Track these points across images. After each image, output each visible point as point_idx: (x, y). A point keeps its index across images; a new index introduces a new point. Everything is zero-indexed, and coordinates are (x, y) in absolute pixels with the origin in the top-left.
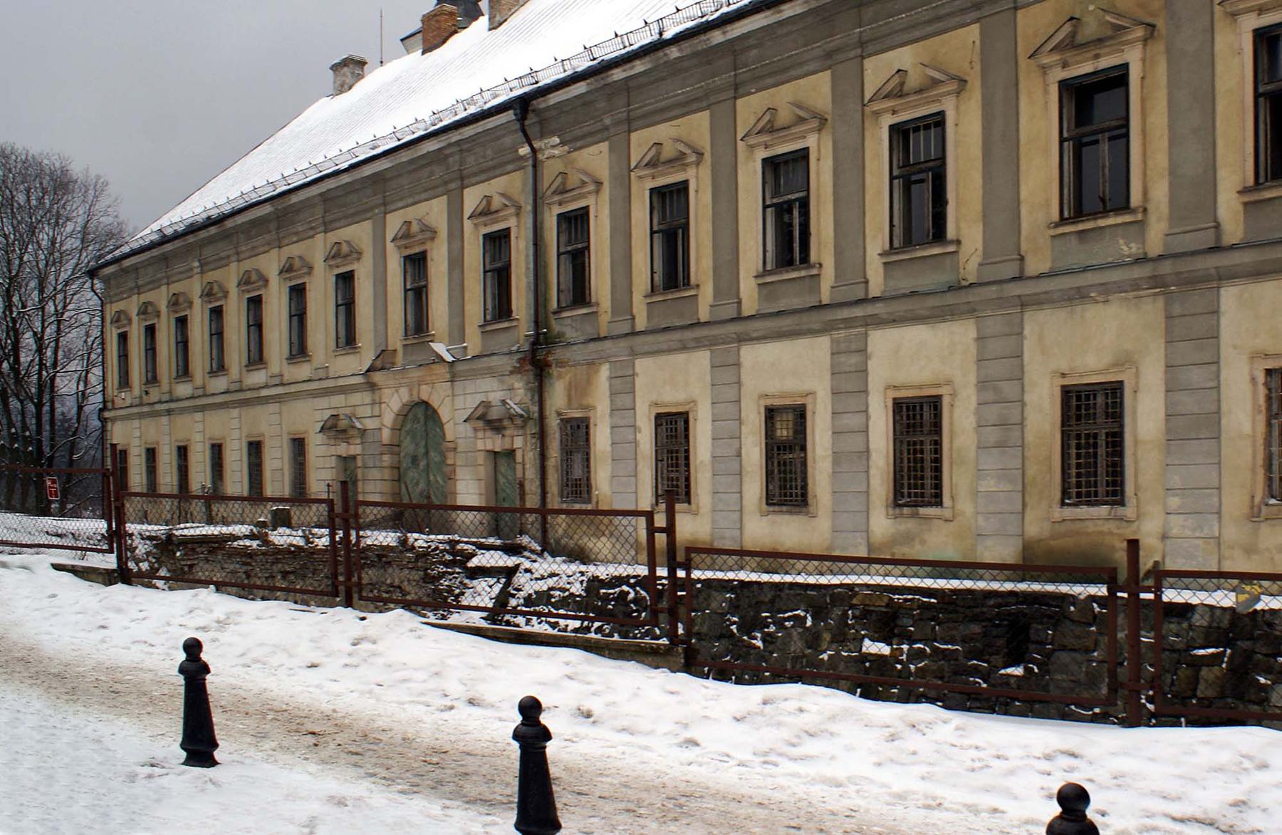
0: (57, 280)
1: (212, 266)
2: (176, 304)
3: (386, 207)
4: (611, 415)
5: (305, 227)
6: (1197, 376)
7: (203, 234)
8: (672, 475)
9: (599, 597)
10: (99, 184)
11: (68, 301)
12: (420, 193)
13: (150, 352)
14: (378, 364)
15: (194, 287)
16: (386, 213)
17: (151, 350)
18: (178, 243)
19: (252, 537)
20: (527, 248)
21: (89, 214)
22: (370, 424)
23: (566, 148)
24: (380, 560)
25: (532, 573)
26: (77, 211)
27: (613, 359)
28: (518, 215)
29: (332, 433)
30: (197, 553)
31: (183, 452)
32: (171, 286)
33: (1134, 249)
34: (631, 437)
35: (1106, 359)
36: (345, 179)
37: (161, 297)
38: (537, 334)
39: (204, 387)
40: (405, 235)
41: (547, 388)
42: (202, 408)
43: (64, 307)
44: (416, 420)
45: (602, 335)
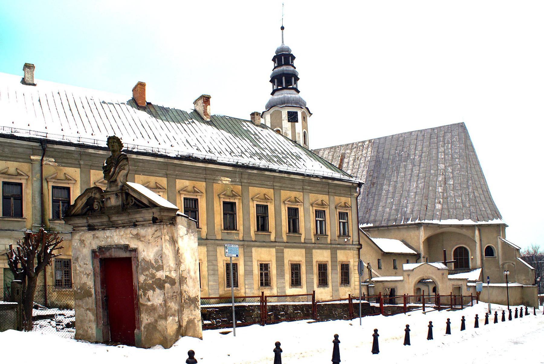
6: (249, 263)
23: (57, 164)
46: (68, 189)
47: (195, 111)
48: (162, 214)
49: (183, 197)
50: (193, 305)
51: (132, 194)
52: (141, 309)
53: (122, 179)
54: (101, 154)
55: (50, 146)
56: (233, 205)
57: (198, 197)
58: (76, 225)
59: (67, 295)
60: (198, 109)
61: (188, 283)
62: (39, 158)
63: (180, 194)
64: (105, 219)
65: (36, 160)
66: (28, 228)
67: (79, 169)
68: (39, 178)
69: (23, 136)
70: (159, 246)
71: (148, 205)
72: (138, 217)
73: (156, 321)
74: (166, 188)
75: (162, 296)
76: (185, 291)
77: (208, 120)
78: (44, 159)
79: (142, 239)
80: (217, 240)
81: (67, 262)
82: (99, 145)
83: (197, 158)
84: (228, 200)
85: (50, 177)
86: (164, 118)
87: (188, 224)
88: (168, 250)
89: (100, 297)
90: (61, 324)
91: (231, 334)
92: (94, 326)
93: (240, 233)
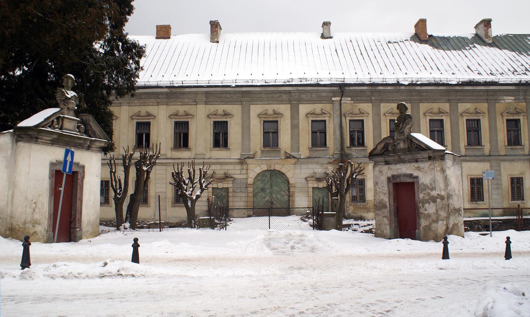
23: (352, 102)
33: (522, 153)
35: (519, 173)
46: (362, 121)
47: (476, 35)
48: (435, 154)
49: (465, 118)
50: (457, 213)
51: (414, 141)
52: (421, 216)
53: (407, 130)
54: (389, 90)
55: (347, 88)
56: (517, 121)
57: (481, 118)
58: (377, 161)
59: (361, 208)
60: (479, 33)
61: (454, 198)
62: (339, 99)
63: (463, 116)
64: (396, 158)
65: (337, 101)
66: (331, 155)
67: (371, 104)
68: (339, 115)
69: (326, 83)
70: (433, 175)
71: (425, 148)
72: (419, 156)
73: (430, 224)
74: (449, 112)
75: (435, 207)
76: (451, 204)
77: (490, 42)
78: (343, 99)
79: (422, 170)
80: (501, 156)
81: (362, 181)
82: (387, 82)
83: (478, 82)
84: (512, 118)
85: (347, 113)
86: (445, 47)
87: (453, 159)
88: (439, 177)
89: (392, 208)
91: (489, 235)
92: (388, 227)
93: (526, 148)
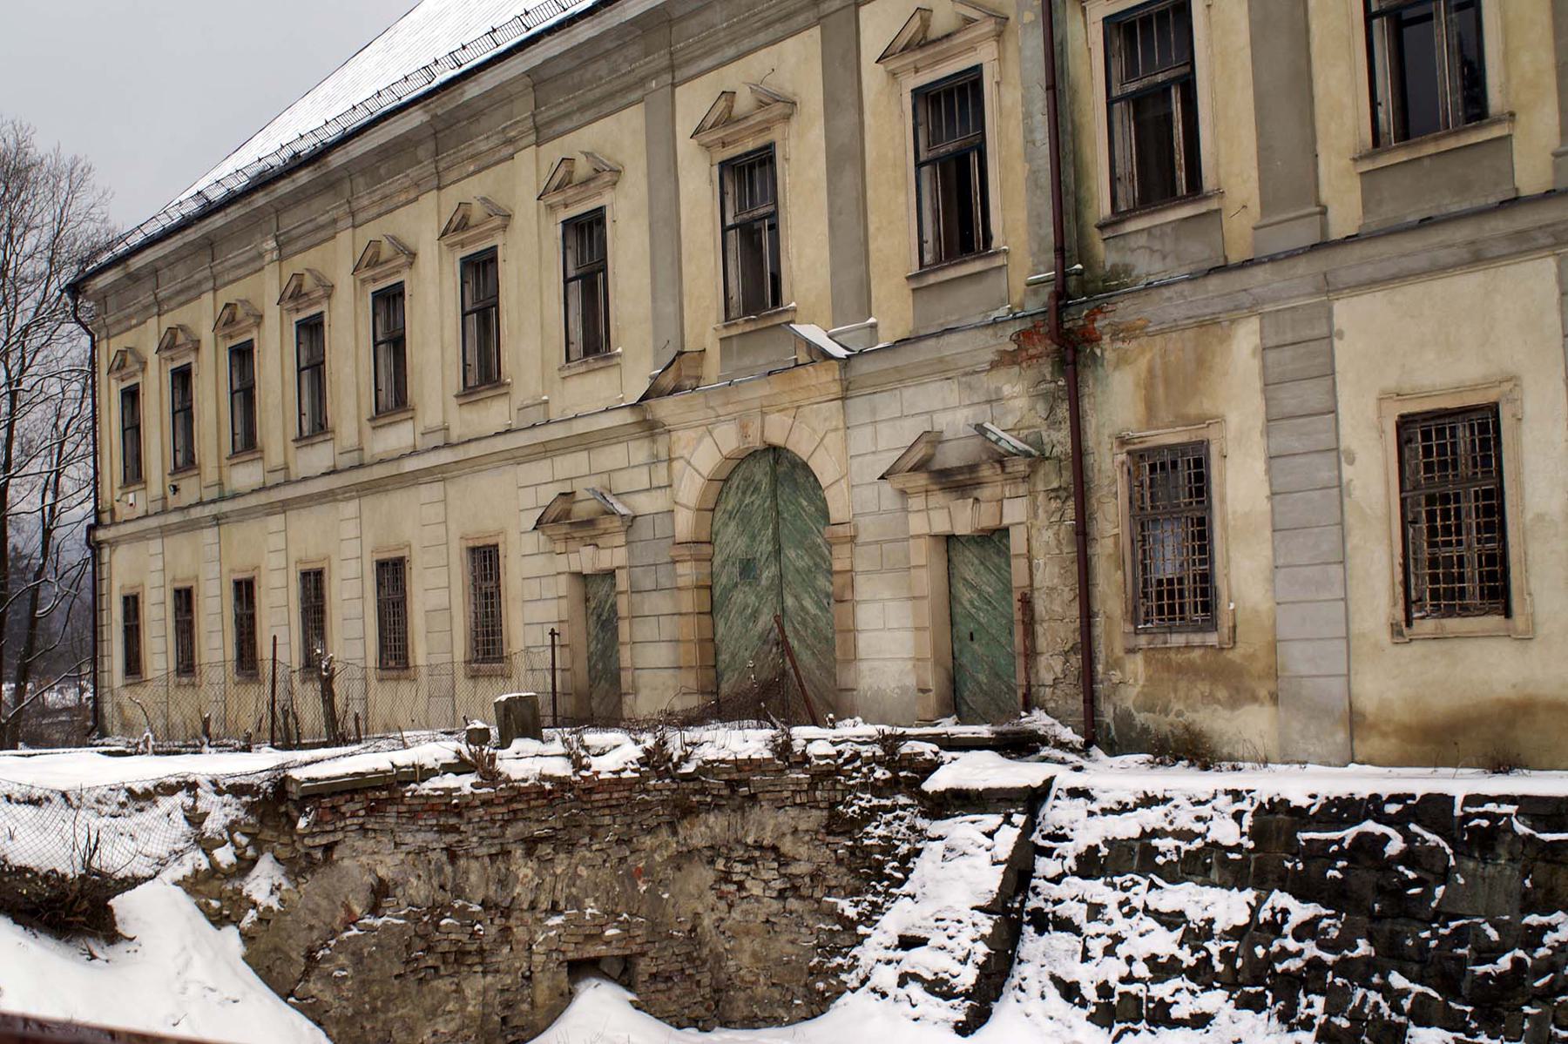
0: (9, 330)
1: (299, 244)
2: (231, 321)
3: (675, 73)
4: (1267, 433)
5: (494, 141)
7: (284, 187)
8: (1444, 552)
9: (1295, 851)
10: (77, 172)
11: (27, 362)
12: (759, 30)
13: (180, 417)
14: (668, 381)
15: (266, 288)
16: (674, 85)
17: (183, 412)
18: (234, 212)
19: (460, 766)
20: (1026, 101)
21: (61, 220)
22: (645, 504)
24: (734, 791)
25: (1092, 799)
26: (42, 213)
27: (1268, 308)
28: (999, 36)
29: (564, 529)
30: (343, 816)
31: (245, 591)
32: (221, 293)
34: (1326, 475)
36: (584, 31)
37: (201, 315)
38: (1063, 275)
39: (286, 468)
40: (725, 118)
41: (1089, 388)
42: (284, 506)
43: (22, 371)
44: (751, 486)
45: (1234, 258)
90: (1061, 847)
